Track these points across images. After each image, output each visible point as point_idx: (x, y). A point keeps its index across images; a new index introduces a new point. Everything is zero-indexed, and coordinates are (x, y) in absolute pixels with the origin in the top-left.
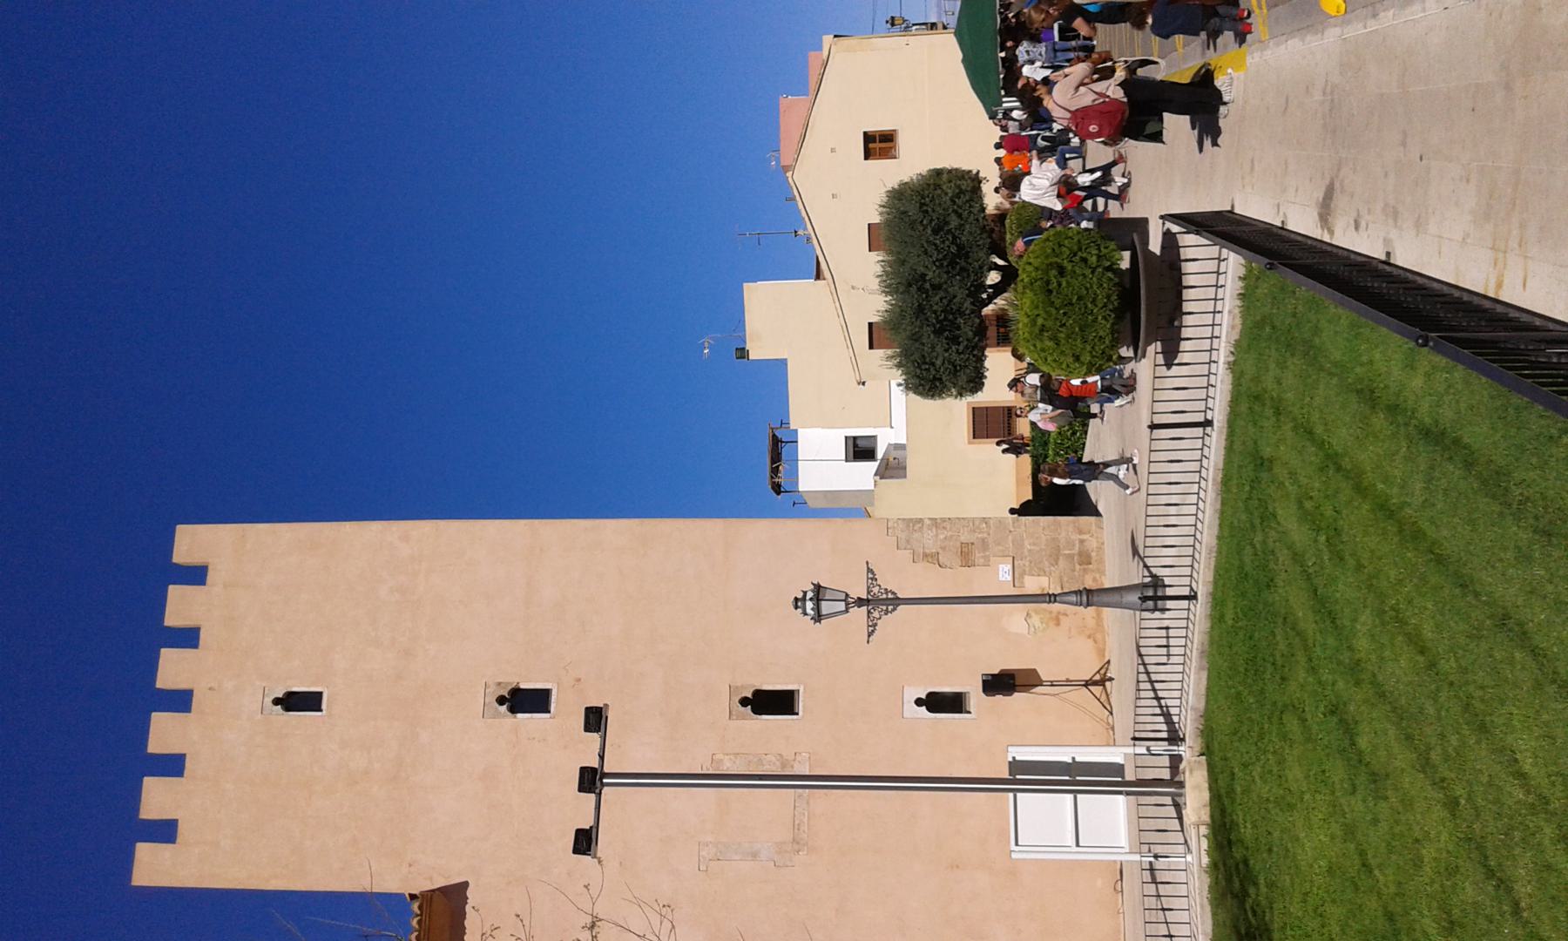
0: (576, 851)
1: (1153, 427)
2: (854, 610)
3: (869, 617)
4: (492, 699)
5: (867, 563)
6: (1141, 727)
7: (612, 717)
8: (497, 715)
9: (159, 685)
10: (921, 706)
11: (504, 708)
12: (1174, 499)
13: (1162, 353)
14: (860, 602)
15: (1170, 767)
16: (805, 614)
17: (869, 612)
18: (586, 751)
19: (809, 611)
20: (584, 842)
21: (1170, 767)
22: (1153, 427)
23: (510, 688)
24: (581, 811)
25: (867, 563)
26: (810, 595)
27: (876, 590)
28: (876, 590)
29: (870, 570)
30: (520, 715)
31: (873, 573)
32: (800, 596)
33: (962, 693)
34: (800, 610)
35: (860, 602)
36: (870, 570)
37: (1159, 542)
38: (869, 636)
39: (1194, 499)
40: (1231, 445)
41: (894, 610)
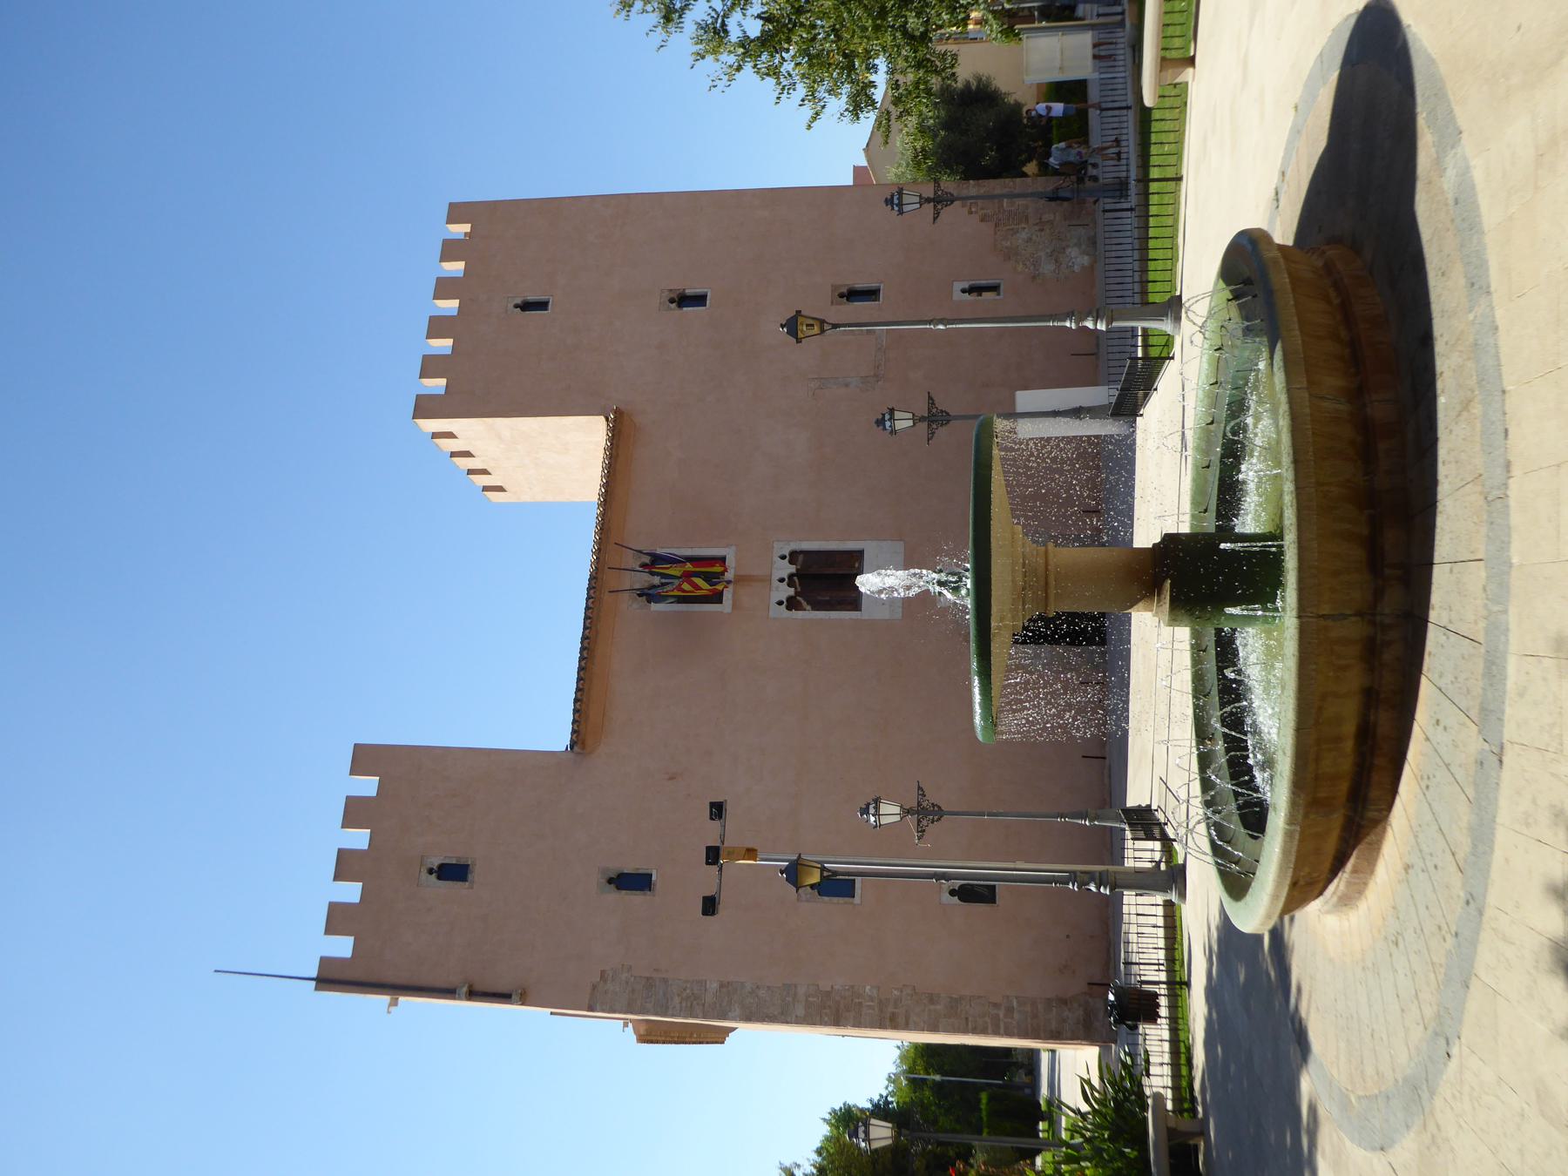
2: (926, 205)
3: (918, 825)
4: (666, 300)
5: (929, 393)
6: (1106, 126)
9: (352, 938)
10: (955, 896)
11: (674, 305)
13: (1149, 336)
14: (928, 200)
16: (885, 429)
17: (919, 821)
18: (711, 833)
19: (887, 427)
20: (717, 810)
23: (678, 292)
25: (929, 393)
26: (887, 417)
28: (934, 411)
29: (920, 788)
30: (685, 309)
34: (881, 427)
35: (928, 200)
36: (920, 788)
41: (939, 819)
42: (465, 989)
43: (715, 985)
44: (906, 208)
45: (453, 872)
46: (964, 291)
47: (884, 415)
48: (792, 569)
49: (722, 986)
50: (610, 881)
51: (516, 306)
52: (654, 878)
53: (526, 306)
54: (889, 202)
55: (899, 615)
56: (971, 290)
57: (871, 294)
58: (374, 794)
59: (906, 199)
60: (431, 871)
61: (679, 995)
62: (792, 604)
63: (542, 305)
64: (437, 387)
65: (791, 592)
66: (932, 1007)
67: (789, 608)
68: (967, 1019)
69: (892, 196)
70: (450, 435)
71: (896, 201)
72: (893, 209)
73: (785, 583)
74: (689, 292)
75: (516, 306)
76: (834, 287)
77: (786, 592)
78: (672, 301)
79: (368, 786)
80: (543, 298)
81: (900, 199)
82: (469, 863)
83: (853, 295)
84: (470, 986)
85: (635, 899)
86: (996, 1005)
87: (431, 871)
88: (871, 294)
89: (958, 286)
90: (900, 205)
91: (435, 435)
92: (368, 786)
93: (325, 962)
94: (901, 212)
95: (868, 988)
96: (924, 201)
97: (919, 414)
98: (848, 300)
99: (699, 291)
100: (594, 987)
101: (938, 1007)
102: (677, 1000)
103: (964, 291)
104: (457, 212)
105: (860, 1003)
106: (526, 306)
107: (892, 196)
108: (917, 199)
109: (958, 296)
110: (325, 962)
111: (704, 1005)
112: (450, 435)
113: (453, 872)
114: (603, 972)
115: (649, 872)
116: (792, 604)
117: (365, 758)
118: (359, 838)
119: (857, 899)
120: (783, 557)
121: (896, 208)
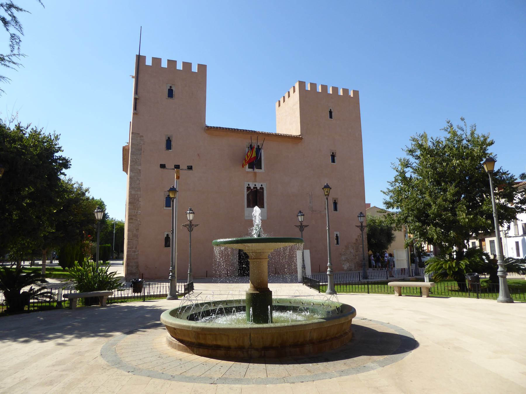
0: (161, 165)
1: (359, 273)
4: (333, 151)
7: (191, 171)
8: (331, 153)
11: (332, 154)
12: (382, 275)
14: (362, 224)
15: (65, 290)
16: (298, 213)
20: (190, 168)
21: (65, 290)
22: (359, 273)
24: (170, 165)
26: (302, 214)
27: (193, 227)
29: (197, 225)
30: (331, 157)
31: (197, 226)
32: (302, 212)
33: (485, 241)
35: (362, 224)
36: (197, 225)
37: (347, 276)
38: (296, 226)
39: (371, 278)
40: (129, 298)
41: (188, 230)
42: (137, 97)
43: (140, 168)
44: (359, 218)
45: (171, 93)
46: (337, 235)
47: (302, 213)
48: (258, 188)
49: (140, 170)
50: (169, 138)
51: (331, 110)
52: (170, 150)
53: (331, 112)
54: (361, 213)
55: (246, 218)
56: (337, 237)
57: (336, 209)
58: (192, 71)
59: (362, 218)
60: (171, 87)
61: (137, 158)
62: (249, 188)
63: (331, 117)
64: (308, 88)
65: (252, 188)
66: (135, 230)
67: (247, 187)
68: (132, 240)
69: (363, 214)
70: (294, 91)
71: (361, 215)
72: (359, 214)
73: (248, 186)
74: (335, 158)
75: (331, 110)
76: (337, 199)
77: (252, 186)
78: (333, 153)
79: (195, 69)
80: (333, 117)
81: (362, 216)
82: (173, 98)
83: (335, 204)
84: (138, 99)
85: (164, 145)
86: (136, 248)
87: (171, 87)
88: (336, 209)
89: (338, 233)
90: (360, 216)
91: (294, 87)
92: (195, 69)
93: (144, 57)
94: (358, 217)
95: (140, 211)
96: (362, 223)
97: (303, 223)
98: (334, 202)
99: (336, 161)
100: (138, 134)
101: (135, 232)
102: (135, 157)
103: (337, 235)
104: (356, 93)
105: (135, 209)
106: (331, 112)
107: (363, 214)
108: (362, 221)
109: (335, 233)
110: (144, 57)
111: (134, 165)
112: (294, 91)
113: (171, 93)
114: (143, 136)
115: (172, 149)
116: (249, 188)
117: (202, 68)
118: (180, 67)
119: (165, 208)
120: (262, 186)
121: (359, 215)
